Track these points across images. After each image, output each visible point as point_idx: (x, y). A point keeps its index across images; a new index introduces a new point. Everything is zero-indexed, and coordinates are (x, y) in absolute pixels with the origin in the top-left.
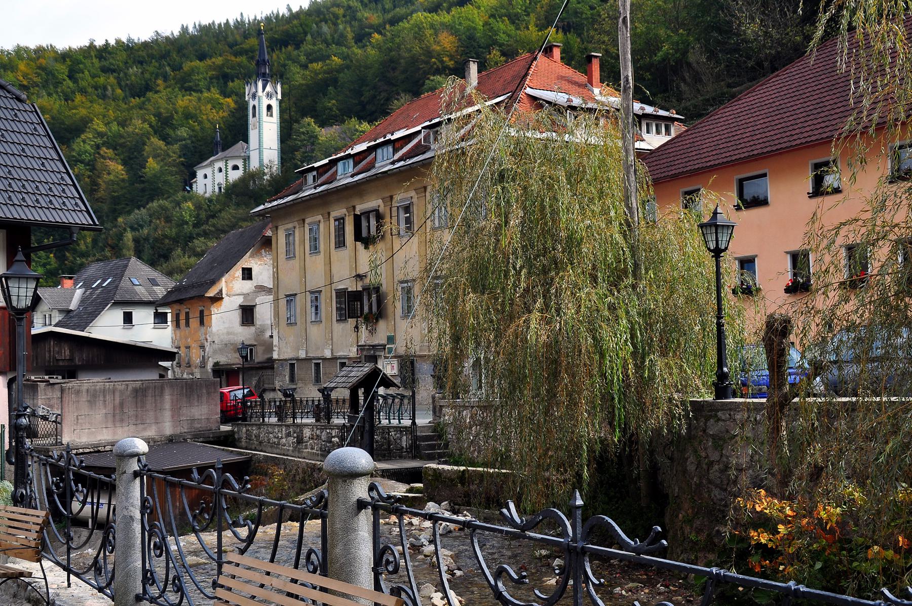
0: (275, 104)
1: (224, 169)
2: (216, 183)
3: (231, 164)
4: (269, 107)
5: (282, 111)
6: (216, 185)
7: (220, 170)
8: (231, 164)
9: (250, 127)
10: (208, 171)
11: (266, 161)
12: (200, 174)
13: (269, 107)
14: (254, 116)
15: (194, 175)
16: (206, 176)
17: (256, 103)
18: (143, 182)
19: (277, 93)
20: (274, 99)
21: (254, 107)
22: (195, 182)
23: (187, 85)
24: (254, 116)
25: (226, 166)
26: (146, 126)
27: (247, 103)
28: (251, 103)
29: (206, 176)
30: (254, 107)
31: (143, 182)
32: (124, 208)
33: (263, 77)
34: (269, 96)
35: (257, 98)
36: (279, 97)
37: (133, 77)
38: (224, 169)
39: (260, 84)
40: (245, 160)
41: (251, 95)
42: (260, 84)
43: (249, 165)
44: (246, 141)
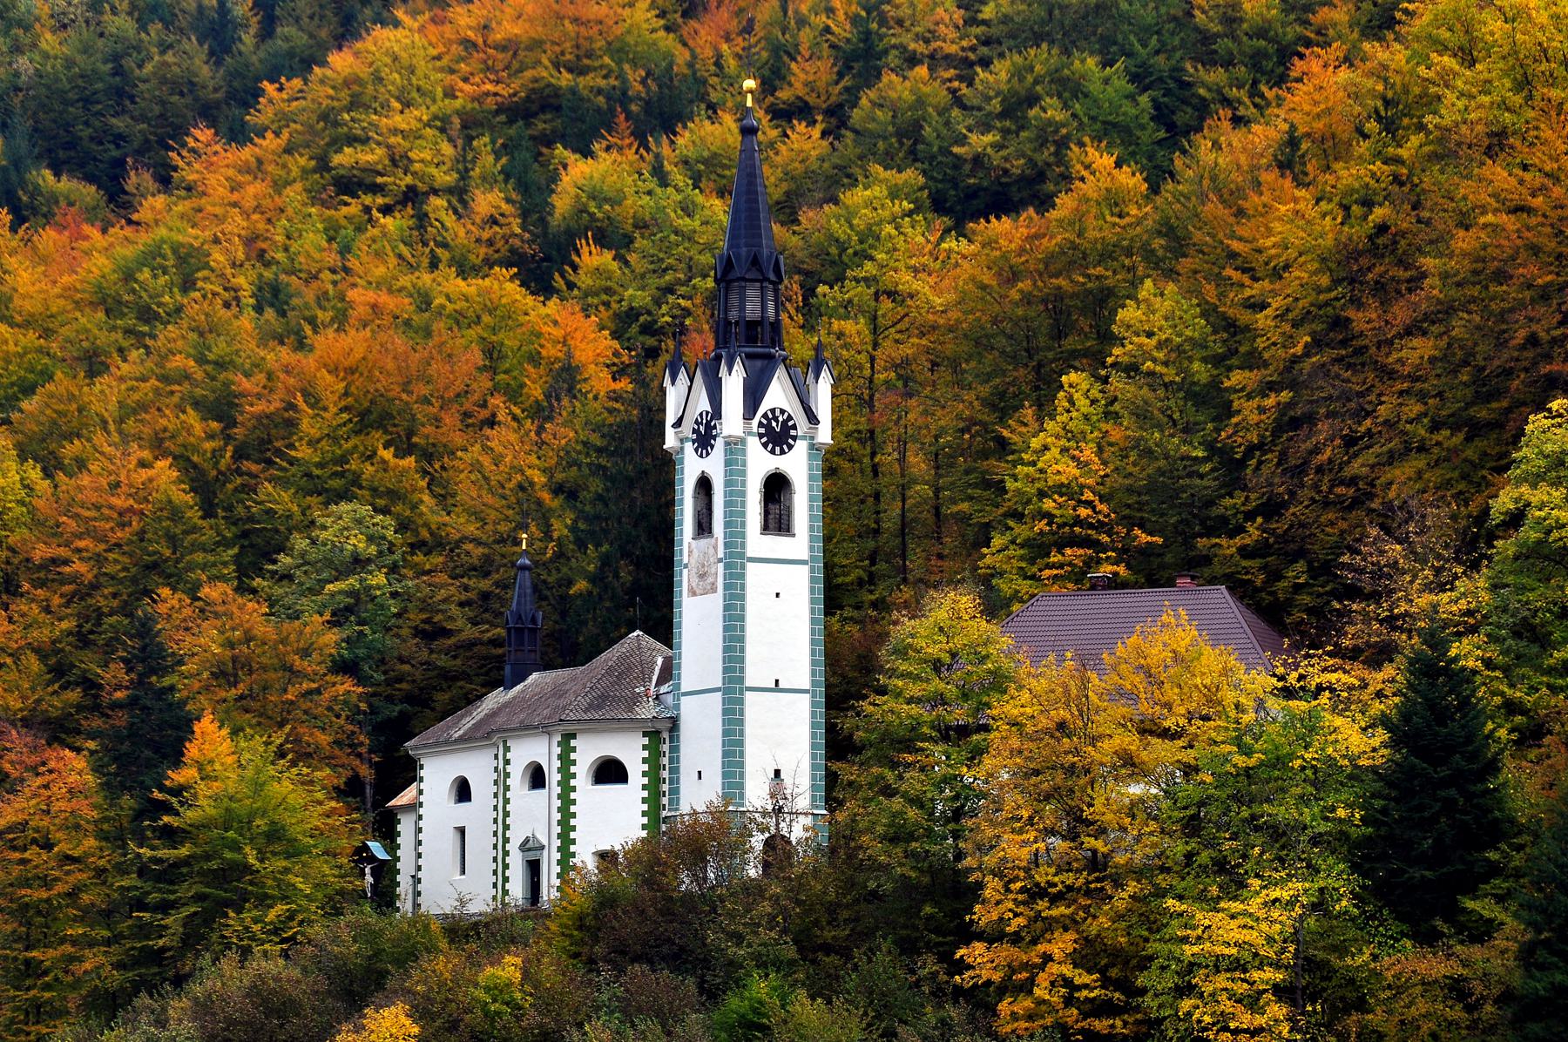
0: (797, 464)
1: (554, 777)
2: (516, 837)
3: (588, 752)
4: (776, 486)
5: (832, 504)
6: (513, 847)
7: (537, 778)
8: (588, 752)
9: (685, 579)
10: (477, 767)
11: (756, 795)
12: (436, 775)
13: (776, 486)
14: (703, 527)
15: (407, 772)
16: (463, 791)
17: (714, 466)
18: (171, 836)
19: (812, 418)
20: (801, 447)
21: (704, 484)
22: (414, 807)
23: (345, 158)
24: (703, 527)
25: (566, 762)
26: (164, 472)
27: (667, 465)
28: (692, 466)
29: (463, 791)
30: (704, 484)
31: (171, 836)
32: (71, 959)
33: (751, 339)
34: (778, 436)
35: (719, 444)
36: (824, 434)
37: (49, 41)
38: (554, 777)
39: (733, 384)
40: (654, 736)
41: (687, 428)
42: (733, 384)
43: (675, 760)
44: (663, 628)
